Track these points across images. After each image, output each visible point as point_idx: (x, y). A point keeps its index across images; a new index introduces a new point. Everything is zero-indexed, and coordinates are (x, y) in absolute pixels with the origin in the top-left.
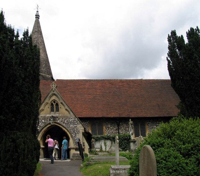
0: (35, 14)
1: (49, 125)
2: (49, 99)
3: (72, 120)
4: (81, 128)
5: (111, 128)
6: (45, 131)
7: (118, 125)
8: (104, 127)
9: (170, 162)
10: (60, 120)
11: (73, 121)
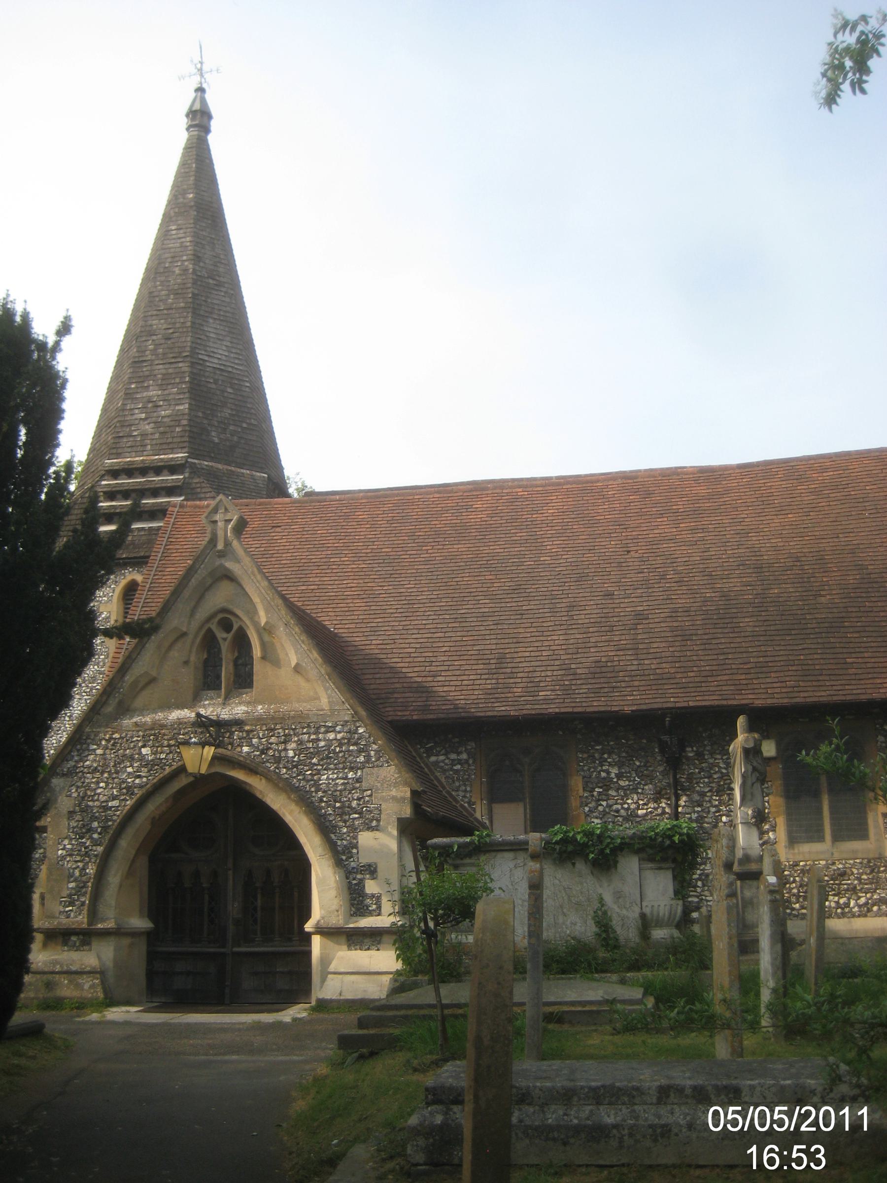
0: (185, 109)
3: (331, 736)
4: (394, 792)
6: (154, 822)
7: (674, 763)
8: (577, 783)
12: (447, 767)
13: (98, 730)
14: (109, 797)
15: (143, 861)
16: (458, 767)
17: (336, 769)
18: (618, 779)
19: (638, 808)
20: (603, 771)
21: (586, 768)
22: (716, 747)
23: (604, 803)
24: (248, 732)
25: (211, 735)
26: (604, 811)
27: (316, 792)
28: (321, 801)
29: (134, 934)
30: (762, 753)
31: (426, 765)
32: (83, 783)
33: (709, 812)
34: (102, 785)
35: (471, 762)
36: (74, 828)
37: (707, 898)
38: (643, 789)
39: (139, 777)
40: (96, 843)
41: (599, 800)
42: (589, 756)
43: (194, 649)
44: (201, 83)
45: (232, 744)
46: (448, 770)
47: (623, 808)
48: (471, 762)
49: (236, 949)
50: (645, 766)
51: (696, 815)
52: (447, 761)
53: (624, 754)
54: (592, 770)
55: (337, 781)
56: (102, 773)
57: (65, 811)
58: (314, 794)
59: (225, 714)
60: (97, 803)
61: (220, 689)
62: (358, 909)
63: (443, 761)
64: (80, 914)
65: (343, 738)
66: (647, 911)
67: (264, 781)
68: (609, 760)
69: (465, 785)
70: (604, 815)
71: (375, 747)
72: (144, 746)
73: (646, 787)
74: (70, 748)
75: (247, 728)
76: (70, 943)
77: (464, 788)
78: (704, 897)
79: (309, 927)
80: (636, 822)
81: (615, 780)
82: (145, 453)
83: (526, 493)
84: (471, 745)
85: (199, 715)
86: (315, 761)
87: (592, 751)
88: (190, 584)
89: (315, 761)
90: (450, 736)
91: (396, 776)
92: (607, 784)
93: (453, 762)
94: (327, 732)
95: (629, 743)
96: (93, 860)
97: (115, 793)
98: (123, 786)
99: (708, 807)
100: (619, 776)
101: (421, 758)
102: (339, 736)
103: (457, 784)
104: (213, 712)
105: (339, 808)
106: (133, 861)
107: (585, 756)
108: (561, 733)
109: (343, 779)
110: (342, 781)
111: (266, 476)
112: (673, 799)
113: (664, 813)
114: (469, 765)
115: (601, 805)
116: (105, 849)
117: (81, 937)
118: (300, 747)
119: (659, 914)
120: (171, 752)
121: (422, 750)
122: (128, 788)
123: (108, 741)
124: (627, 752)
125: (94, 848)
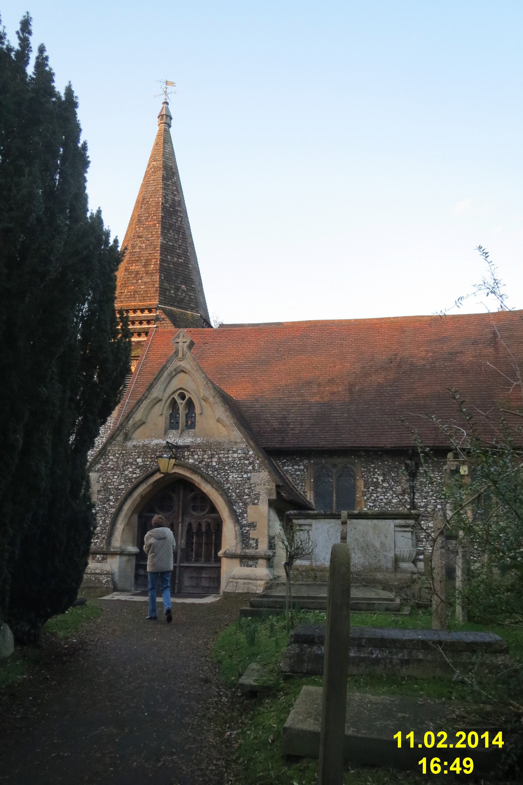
1: (158, 476)
2: (163, 387)
3: (235, 455)
5: (385, 485)
6: (143, 497)
7: (413, 475)
8: (360, 484)
9: (463, 753)
10: (196, 457)
11: (240, 459)
12: (293, 473)
13: (114, 448)
14: (119, 484)
15: (136, 517)
16: (299, 473)
17: (237, 472)
18: (383, 483)
19: (393, 499)
20: (375, 478)
21: (366, 476)
22: (435, 468)
23: (375, 495)
24: (192, 452)
25: (173, 453)
26: (375, 499)
27: (227, 484)
28: (229, 488)
29: (130, 554)
30: (460, 473)
31: (282, 471)
32: (106, 476)
33: (431, 502)
34: (116, 477)
35: (305, 470)
36: (100, 499)
37: (429, 548)
38: (396, 489)
39: (135, 473)
40: (111, 507)
41: (372, 493)
42: (368, 470)
43: (166, 408)
44: (166, 99)
45: (184, 458)
46: (293, 474)
47: (385, 498)
48: (305, 470)
49: (182, 565)
50: (397, 476)
51: (424, 504)
52: (293, 470)
53: (386, 470)
54: (369, 477)
55: (237, 479)
56: (116, 470)
57: (96, 490)
58: (225, 485)
59: (181, 442)
60: (113, 486)
61: (179, 429)
62: (246, 546)
63: (291, 469)
64: (101, 544)
65: (242, 457)
66: (398, 553)
67: (200, 477)
68: (378, 472)
69: (302, 483)
70: (375, 501)
71: (258, 462)
72: (138, 458)
73: (397, 488)
74: (99, 457)
75: (192, 450)
76: (96, 559)
77: (301, 484)
78: (426, 548)
79: (220, 553)
80: (392, 506)
81: (381, 483)
82: (136, 301)
83: (338, 329)
84: (306, 462)
85: (167, 443)
86: (226, 468)
87: (369, 467)
88: (164, 374)
89: (226, 468)
90: (295, 457)
91: (268, 477)
92: (376, 485)
93: (296, 470)
94: (234, 453)
95: (389, 464)
96: (109, 516)
97: (122, 481)
98: (127, 478)
99: (430, 500)
100: (383, 481)
101: (279, 467)
102: (239, 456)
103: (298, 482)
104: (174, 441)
105: (238, 492)
106: (130, 517)
107: (366, 470)
108: (353, 457)
109: (241, 477)
110: (240, 479)
111: (199, 315)
112: (412, 494)
113: (406, 501)
114: (304, 472)
115: (373, 496)
116: (116, 510)
117: (102, 556)
118: (219, 461)
119: (404, 555)
120: (152, 461)
121: (280, 463)
122: (129, 479)
123: (120, 454)
124: (388, 469)
125: (110, 510)
